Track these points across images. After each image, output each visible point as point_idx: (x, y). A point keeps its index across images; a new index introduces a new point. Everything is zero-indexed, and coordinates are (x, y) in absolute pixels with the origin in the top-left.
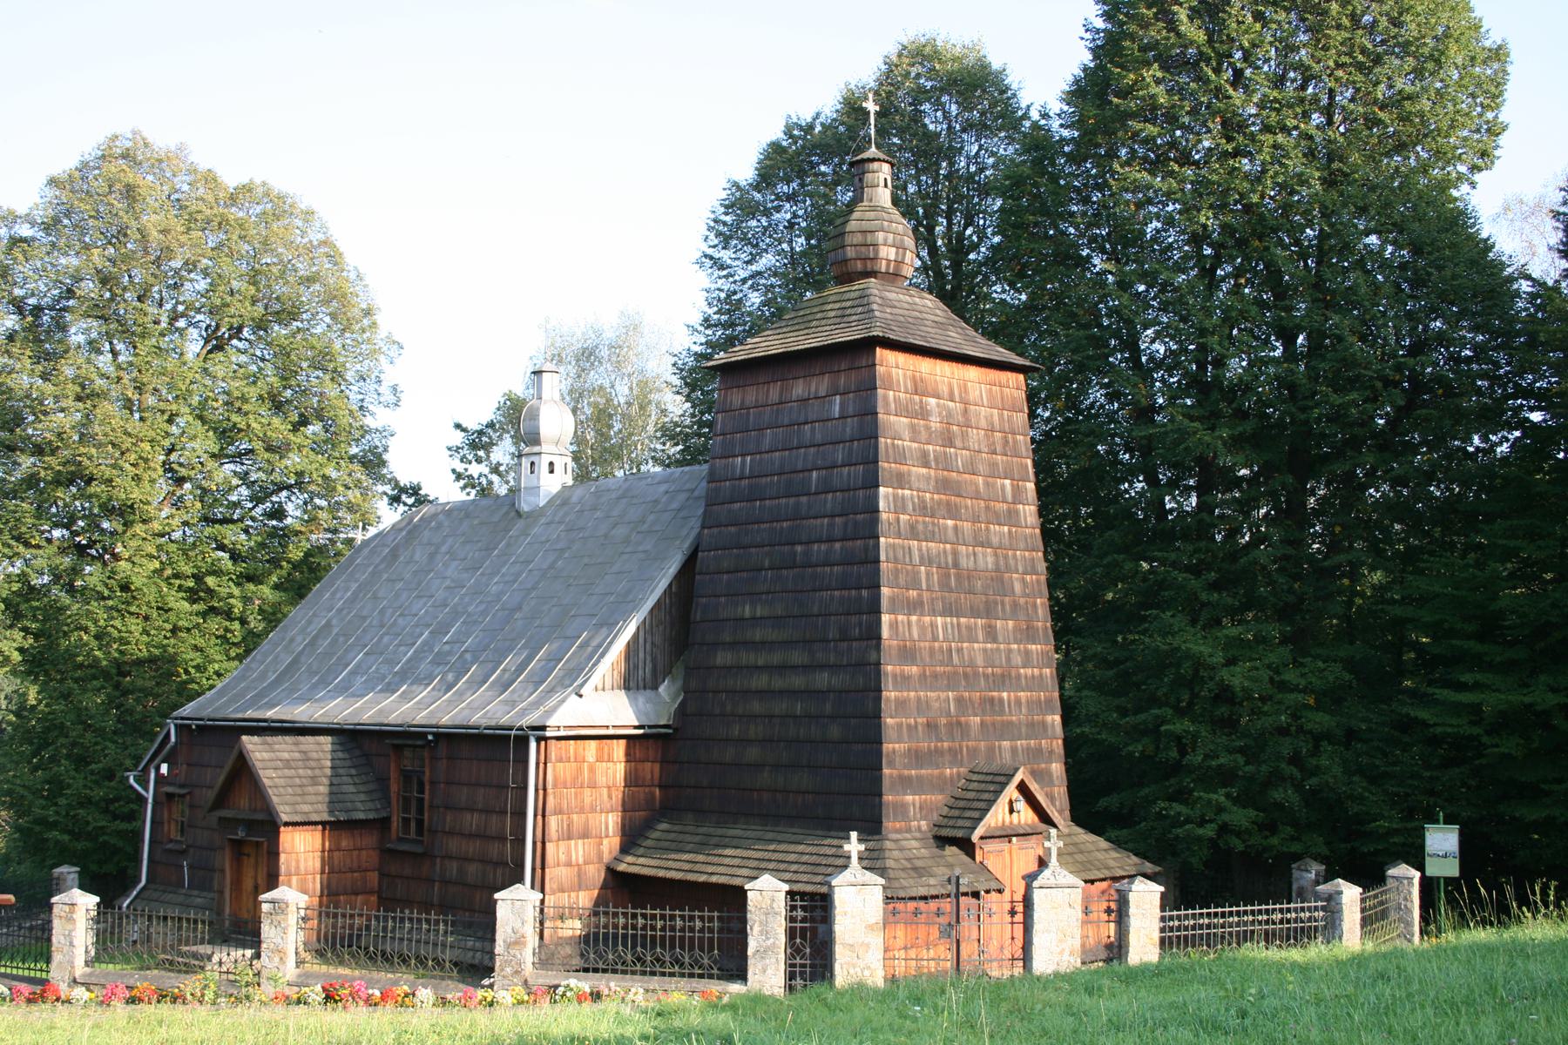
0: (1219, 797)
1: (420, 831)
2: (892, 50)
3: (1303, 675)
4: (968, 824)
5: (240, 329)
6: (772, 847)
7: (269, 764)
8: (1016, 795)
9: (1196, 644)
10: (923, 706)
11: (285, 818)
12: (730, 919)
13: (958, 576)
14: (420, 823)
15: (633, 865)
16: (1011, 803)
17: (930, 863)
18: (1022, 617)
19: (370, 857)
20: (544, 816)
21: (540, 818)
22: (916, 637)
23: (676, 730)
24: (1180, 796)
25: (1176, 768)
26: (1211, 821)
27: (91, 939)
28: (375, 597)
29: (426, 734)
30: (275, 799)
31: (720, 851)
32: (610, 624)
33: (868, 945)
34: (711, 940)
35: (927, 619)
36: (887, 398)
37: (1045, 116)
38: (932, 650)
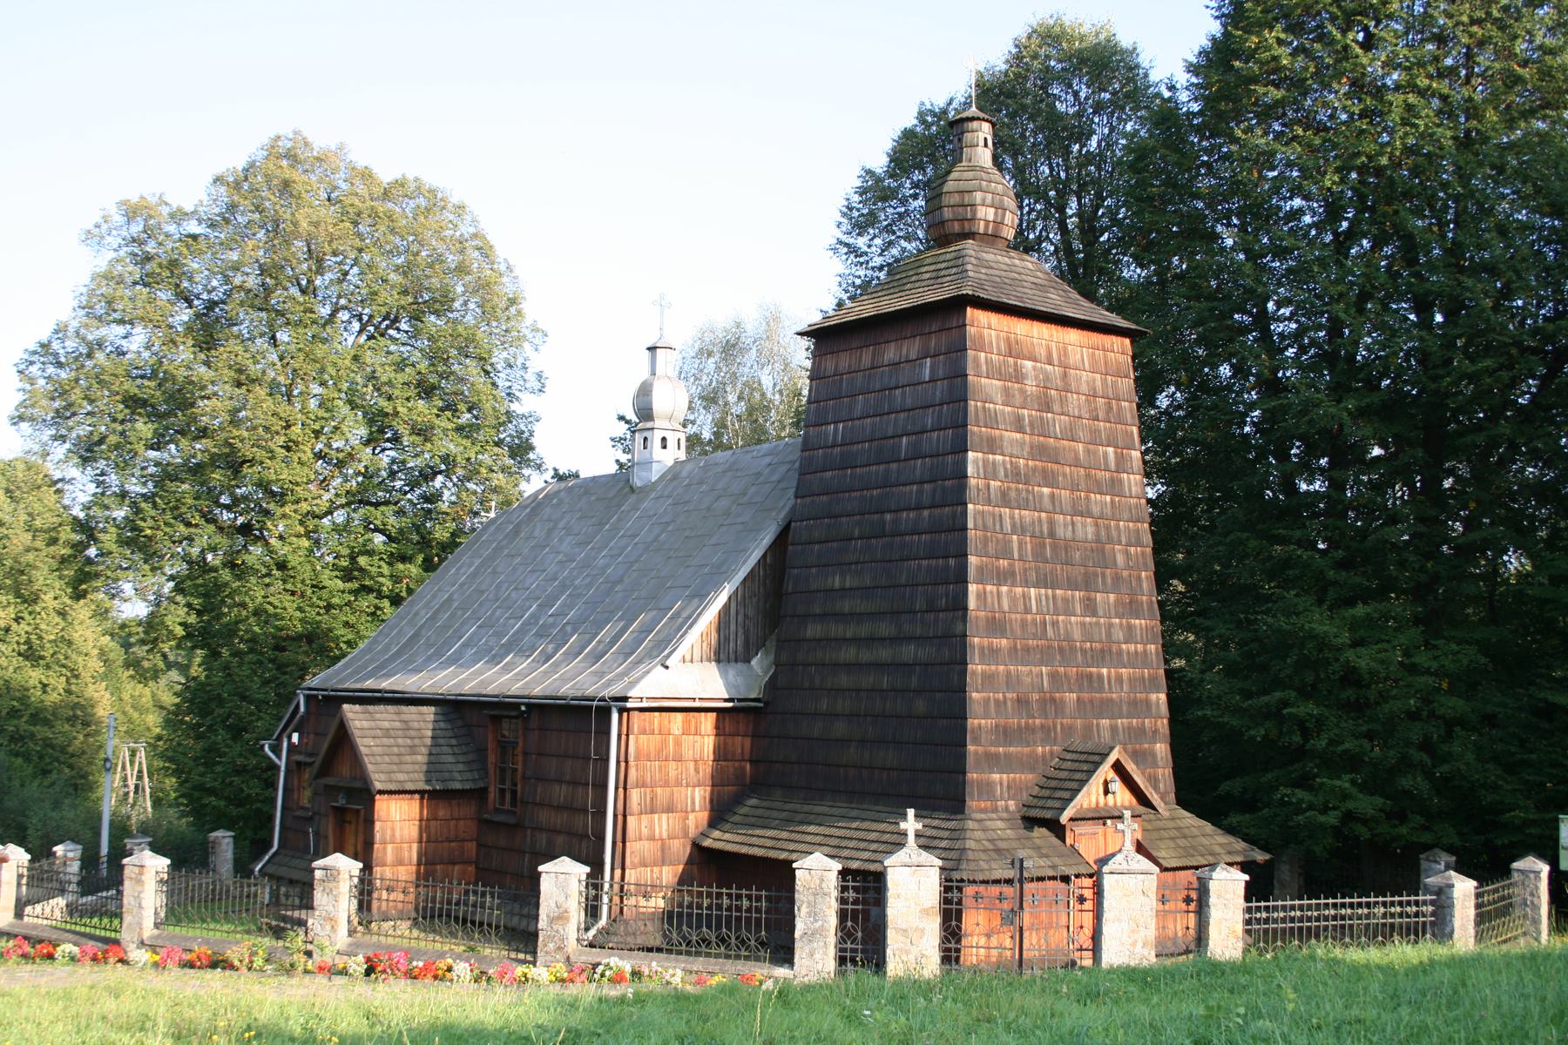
0: (1344, 783)
1: (514, 803)
2: (1021, 32)
3: (1435, 658)
4: (1057, 804)
5: (396, 320)
6: (854, 825)
7: (368, 733)
8: (1111, 775)
9: (1320, 623)
10: (1011, 681)
11: (378, 786)
12: (778, 899)
13: (1054, 547)
14: (514, 793)
15: (721, 840)
16: (1106, 783)
17: (1014, 844)
18: (1124, 590)
19: (467, 827)
20: (625, 789)
21: (621, 790)
22: (1006, 608)
23: (767, 704)
24: (1304, 782)
25: (1301, 753)
26: (1334, 808)
27: (162, 899)
28: (494, 572)
29: (519, 704)
30: (370, 767)
31: (803, 828)
32: (701, 595)
33: (923, 931)
34: (758, 920)
35: (1019, 590)
36: (977, 360)
37: (1172, 88)
38: (1024, 623)
